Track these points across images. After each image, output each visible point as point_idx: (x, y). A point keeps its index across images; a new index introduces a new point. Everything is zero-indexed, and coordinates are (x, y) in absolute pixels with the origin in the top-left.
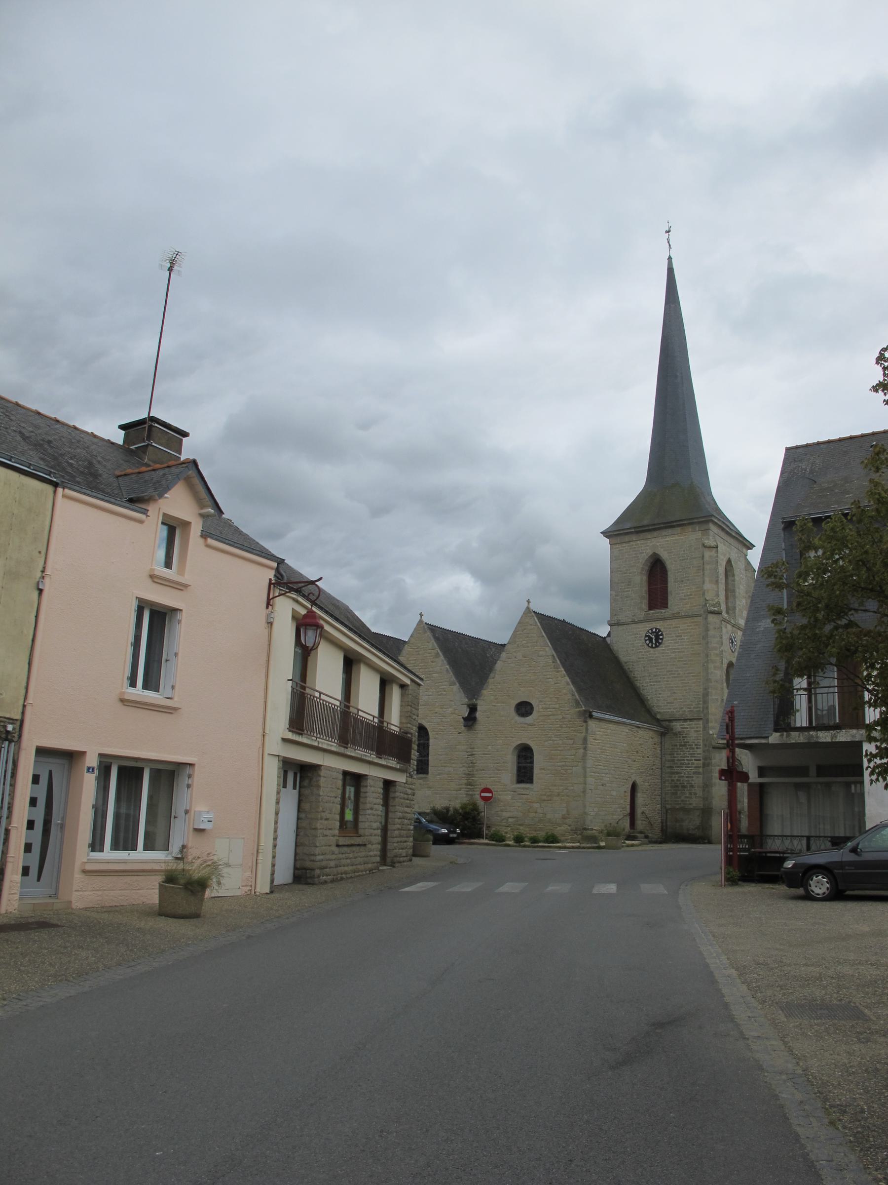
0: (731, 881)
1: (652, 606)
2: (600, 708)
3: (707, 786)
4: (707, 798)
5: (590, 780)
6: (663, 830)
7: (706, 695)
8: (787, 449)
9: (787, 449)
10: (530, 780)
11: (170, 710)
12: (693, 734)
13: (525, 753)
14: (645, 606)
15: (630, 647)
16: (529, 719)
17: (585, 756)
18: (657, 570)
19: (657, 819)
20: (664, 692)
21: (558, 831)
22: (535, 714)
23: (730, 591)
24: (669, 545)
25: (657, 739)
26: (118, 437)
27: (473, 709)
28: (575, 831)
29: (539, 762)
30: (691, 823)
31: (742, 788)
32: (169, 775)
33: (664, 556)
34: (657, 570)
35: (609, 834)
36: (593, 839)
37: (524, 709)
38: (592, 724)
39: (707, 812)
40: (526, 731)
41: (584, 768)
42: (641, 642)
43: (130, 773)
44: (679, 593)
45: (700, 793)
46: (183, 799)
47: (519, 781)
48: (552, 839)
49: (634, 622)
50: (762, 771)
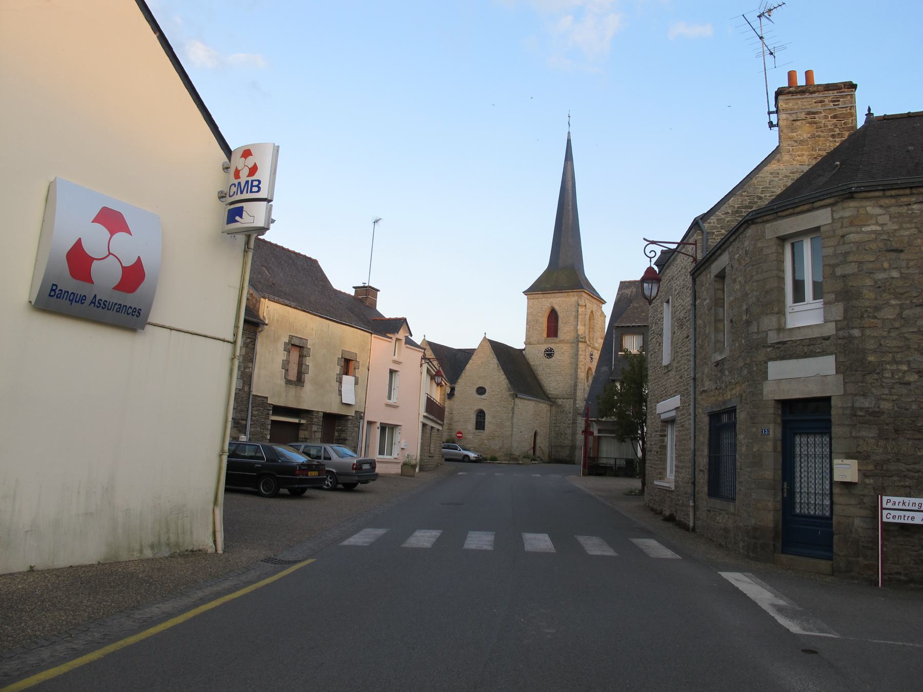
0: (584, 475)
1: (549, 335)
2: (520, 392)
3: (574, 434)
4: (574, 440)
5: (515, 429)
6: (549, 456)
7: (576, 385)
8: (621, 283)
9: (621, 283)
10: (483, 428)
11: (396, 407)
12: (567, 406)
13: (481, 415)
14: (545, 335)
15: (536, 357)
16: (483, 396)
17: (512, 417)
18: (553, 316)
19: (546, 451)
20: (553, 383)
21: (497, 455)
22: (487, 394)
23: (591, 329)
24: (562, 302)
25: (548, 408)
26: (352, 292)
27: (453, 389)
28: (506, 455)
29: (488, 418)
30: (564, 454)
31: (591, 438)
32: (393, 427)
33: (557, 308)
34: (553, 316)
35: (524, 457)
36: (516, 459)
37: (481, 391)
38: (517, 401)
39: (573, 448)
40: (481, 403)
41: (512, 423)
42: (542, 354)
43: (383, 427)
44: (565, 330)
45: (570, 438)
46: (397, 437)
47: (477, 429)
48: (494, 459)
49: (538, 343)
50: (600, 431)
